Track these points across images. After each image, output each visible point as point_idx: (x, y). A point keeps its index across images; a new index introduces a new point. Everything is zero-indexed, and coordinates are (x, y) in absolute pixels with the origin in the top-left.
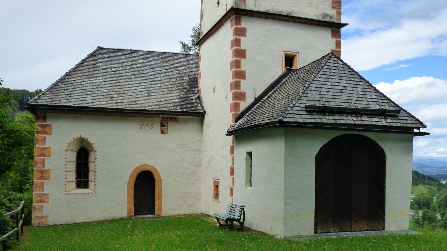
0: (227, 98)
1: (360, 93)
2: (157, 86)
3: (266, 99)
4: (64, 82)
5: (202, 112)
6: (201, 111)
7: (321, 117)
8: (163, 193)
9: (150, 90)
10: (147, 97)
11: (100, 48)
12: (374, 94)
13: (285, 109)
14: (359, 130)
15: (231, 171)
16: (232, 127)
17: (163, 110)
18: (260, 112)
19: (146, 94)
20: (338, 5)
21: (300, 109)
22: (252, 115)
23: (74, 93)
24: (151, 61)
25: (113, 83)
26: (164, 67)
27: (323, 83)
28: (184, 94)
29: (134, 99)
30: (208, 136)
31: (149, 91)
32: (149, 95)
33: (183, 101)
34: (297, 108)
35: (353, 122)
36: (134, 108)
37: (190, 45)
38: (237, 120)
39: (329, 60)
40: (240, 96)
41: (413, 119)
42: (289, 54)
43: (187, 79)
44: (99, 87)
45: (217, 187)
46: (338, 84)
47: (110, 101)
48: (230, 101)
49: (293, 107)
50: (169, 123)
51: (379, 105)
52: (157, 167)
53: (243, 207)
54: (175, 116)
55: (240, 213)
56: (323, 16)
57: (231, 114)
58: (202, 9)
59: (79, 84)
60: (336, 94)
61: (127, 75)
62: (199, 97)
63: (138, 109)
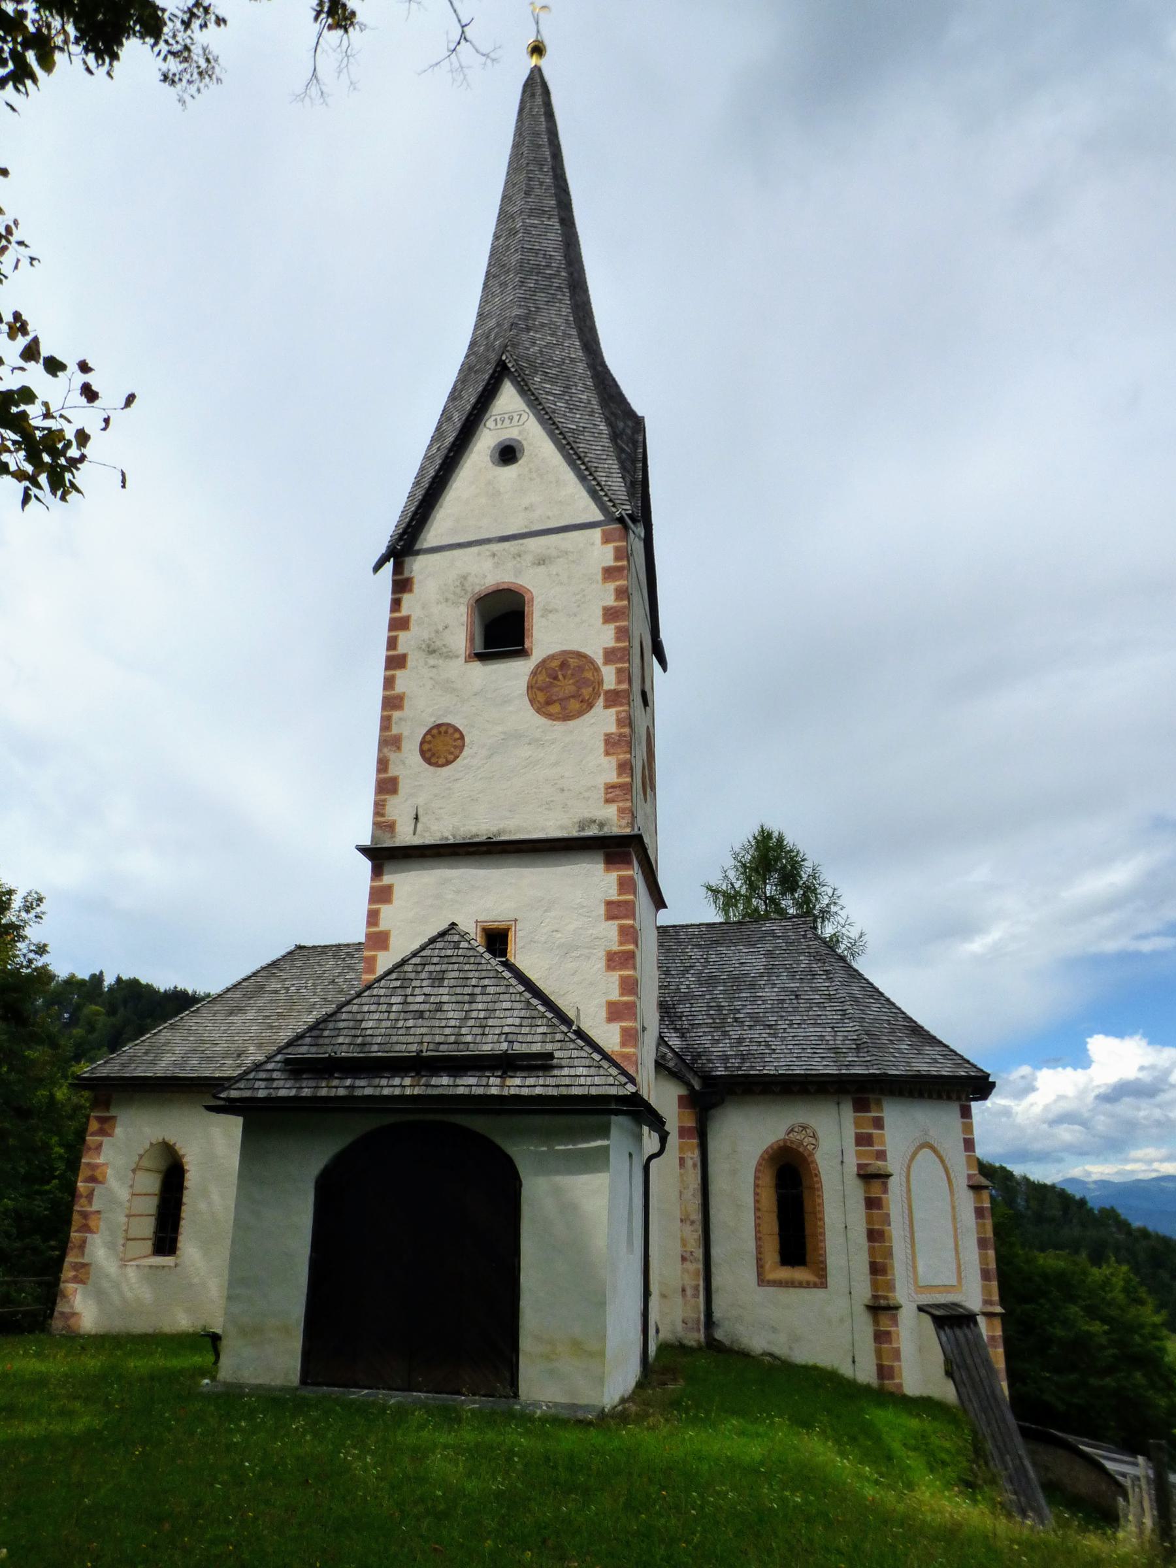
11: (300, 948)
20: (621, 793)
42: (500, 927)
56: (579, 827)
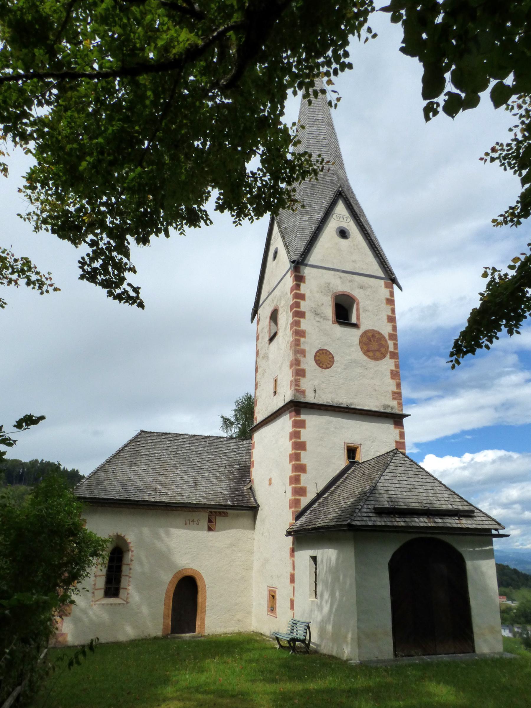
0: (285, 493)
1: (429, 491)
2: (205, 475)
3: (329, 495)
4: (104, 470)
5: (255, 505)
6: (254, 504)
7: (391, 519)
8: (207, 604)
9: (197, 480)
10: (193, 488)
11: (143, 432)
12: (444, 492)
13: (353, 510)
14: (433, 533)
15: (290, 578)
16: (292, 526)
17: (211, 503)
18: (324, 511)
19: (193, 485)
21: (368, 510)
22: (315, 513)
23: (114, 483)
24: (198, 447)
25: (156, 472)
26: (212, 454)
27: (390, 481)
28: (235, 484)
29: (179, 490)
30: (263, 534)
31: (196, 482)
32: (196, 485)
33: (233, 492)
34: (365, 510)
35: (425, 525)
36: (180, 502)
37: (233, 419)
38: (298, 517)
39: (394, 456)
40: (300, 491)
41: (490, 519)
43: (237, 467)
44: (141, 476)
45: (273, 597)
46: (406, 482)
47: (153, 493)
48: (289, 495)
49: (361, 508)
50: (218, 518)
51: (451, 505)
52: (201, 572)
53: (308, 623)
54: (225, 511)
55: (305, 631)
57: (291, 510)
58: (256, 395)
59: (119, 472)
60: (405, 493)
61: (172, 462)
62: (251, 488)
63: (184, 502)
